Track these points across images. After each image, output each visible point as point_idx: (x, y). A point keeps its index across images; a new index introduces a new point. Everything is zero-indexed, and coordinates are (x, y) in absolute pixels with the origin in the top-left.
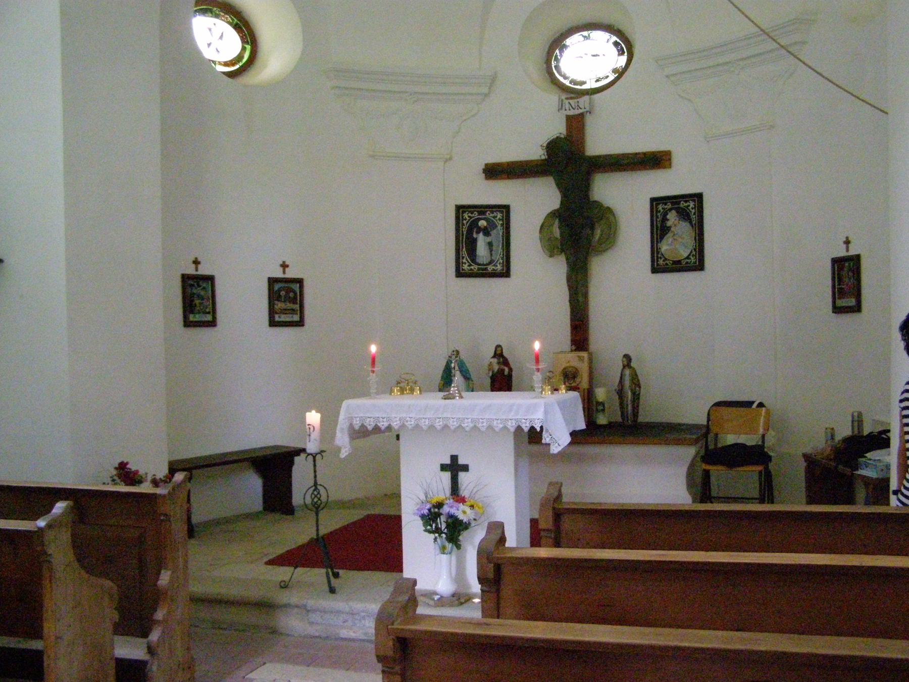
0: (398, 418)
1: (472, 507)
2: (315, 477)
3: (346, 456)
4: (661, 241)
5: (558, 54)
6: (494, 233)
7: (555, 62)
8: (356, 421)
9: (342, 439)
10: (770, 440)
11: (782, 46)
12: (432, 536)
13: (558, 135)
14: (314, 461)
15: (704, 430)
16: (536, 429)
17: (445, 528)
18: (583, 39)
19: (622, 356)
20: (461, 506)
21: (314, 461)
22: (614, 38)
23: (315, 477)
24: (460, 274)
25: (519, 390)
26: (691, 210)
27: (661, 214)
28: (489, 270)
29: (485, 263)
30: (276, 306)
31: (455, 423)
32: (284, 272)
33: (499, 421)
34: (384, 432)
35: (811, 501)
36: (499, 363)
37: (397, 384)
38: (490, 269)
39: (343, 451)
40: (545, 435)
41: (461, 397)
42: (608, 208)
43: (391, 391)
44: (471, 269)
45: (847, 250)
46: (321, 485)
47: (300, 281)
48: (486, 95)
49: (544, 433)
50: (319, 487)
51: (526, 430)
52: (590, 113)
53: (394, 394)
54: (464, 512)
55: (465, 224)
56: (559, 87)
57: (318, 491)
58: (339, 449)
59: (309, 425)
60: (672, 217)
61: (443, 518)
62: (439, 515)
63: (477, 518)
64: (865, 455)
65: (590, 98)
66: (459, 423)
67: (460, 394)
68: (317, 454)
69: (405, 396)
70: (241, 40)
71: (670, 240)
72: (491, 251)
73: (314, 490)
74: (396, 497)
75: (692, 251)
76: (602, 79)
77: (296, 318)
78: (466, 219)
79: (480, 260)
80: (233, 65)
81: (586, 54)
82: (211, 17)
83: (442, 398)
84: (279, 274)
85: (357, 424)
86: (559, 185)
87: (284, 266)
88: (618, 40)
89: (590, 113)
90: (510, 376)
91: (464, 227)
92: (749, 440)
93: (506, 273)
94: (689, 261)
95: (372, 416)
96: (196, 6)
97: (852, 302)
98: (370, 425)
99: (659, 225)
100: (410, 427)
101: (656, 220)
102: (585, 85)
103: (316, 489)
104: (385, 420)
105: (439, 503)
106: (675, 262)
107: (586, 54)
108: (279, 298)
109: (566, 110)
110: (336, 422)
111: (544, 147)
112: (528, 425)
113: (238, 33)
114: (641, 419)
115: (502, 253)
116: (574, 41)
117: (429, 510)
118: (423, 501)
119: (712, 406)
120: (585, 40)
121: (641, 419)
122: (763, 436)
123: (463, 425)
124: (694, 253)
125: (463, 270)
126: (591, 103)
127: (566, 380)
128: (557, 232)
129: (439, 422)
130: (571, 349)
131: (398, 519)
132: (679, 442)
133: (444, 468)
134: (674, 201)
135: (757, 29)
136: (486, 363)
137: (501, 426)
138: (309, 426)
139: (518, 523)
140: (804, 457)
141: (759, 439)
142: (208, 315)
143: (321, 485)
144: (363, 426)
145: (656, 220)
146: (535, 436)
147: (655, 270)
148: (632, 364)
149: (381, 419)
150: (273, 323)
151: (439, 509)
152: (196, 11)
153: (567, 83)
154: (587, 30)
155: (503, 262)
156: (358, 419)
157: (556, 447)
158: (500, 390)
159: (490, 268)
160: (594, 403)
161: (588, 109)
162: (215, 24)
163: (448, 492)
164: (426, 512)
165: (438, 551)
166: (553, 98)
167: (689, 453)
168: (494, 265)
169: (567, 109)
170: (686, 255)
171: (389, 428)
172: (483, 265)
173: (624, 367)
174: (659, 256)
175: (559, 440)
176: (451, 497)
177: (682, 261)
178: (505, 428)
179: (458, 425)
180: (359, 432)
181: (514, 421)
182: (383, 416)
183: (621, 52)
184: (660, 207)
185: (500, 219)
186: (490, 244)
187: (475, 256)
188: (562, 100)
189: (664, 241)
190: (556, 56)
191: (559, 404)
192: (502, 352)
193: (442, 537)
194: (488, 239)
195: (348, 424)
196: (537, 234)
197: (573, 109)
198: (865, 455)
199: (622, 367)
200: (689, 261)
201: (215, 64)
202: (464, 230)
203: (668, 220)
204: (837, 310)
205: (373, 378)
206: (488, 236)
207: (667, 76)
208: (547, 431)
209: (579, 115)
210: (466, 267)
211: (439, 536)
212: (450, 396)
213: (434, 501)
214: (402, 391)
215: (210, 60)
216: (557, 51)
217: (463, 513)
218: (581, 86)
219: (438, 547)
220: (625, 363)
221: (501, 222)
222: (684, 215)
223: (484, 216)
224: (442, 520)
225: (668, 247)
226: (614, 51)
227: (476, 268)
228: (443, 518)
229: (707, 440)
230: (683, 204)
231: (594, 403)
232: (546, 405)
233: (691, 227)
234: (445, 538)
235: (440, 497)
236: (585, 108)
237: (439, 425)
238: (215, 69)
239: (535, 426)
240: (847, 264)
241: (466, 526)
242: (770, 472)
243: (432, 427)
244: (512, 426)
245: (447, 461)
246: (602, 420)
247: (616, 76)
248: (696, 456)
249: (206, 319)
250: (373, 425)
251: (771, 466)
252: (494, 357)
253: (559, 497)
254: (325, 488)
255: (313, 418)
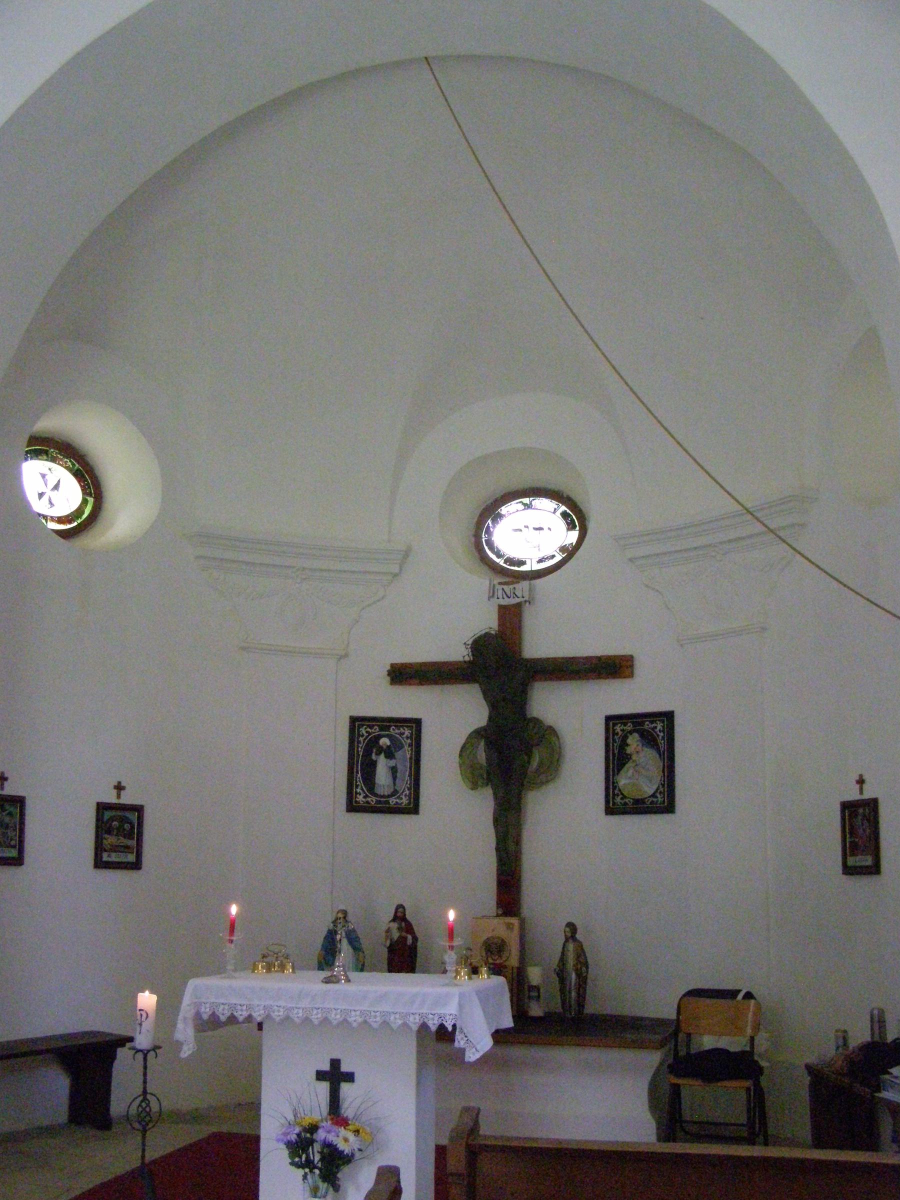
0: (262, 1006)
1: (357, 1132)
2: (145, 1082)
3: (189, 1056)
4: (617, 774)
5: (491, 525)
6: (399, 754)
7: (486, 536)
8: (206, 1008)
9: (185, 1032)
10: (762, 1043)
11: (772, 531)
12: (300, 1172)
13: (487, 631)
14: (145, 1059)
15: (671, 1030)
16: (447, 1028)
17: (319, 1161)
18: (523, 507)
19: (564, 924)
20: (342, 1131)
21: (145, 1059)
22: (563, 508)
23: (145, 1082)
24: (353, 807)
25: (424, 972)
26: (658, 733)
27: (619, 738)
28: (391, 803)
29: (386, 794)
30: (105, 841)
31: (338, 1016)
32: (119, 797)
33: (397, 1016)
34: (240, 1023)
35: (818, 1143)
36: (400, 929)
37: (263, 958)
38: (392, 802)
39: (185, 1048)
40: (458, 1036)
41: (348, 980)
42: (550, 727)
43: (254, 968)
44: (368, 802)
45: (861, 792)
46: (152, 1094)
47: (139, 810)
48: (395, 575)
49: (457, 1033)
50: (149, 1097)
51: (434, 1028)
52: (530, 603)
53: (258, 972)
54: (346, 1140)
55: (362, 742)
56: (490, 567)
57: (147, 1102)
58: (179, 1045)
59: (140, 1010)
60: (634, 741)
61: (317, 1147)
62: (311, 1142)
63: (364, 1149)
64: (889, 1070)
65: (530, 584)
66: (343, 1016)
67: (346, 973)
68: (148, 1051)
69: (273, 975)
70: (82, 490)
71: (631, 771)
72: (394, 778)
73: (142, 1101)
74: (254, 1107)
75: (659, 787)
76: (546, 559)
77: (131, 858)
78: (363, 736)
79: (379, 791)
80: (70, 523)
81: (527, 527)
82: (46, 460)
83: (322, 981)
84: (111, 798)
85: (206, 1013)
86: (485, 694)
87: (119, 788)
88: (568, 511)
89: (530, 603)
90: (413, 949)
91: (360, 745)
92: (734, 1044)
93: (413, 808)
94: (655, 800)
95: (226, 1001)
96: (28, 446)
97: (868, 861)
98: (223, 1014)
99: (616, 752)
100: (278, 1019)
101: (613, 745)
102: (525, 566)
103: (145, 1099)
104: (244, 1008)
105: (312, 1125)
106: (637, 801)
107: (527, 527)
108: (109, 832)
109: (498, 598)
110: (177, 1008)
111: (468, 645)
112: (436, 1022)
113: (79, 482)
114: (591, 1008)
115: (409, 782)
116: (511, 509)
117: (299, 1135)
118: (291, 1123)
119: (684, 995)
120: (525, 509)
121: (591, 1008)
122: (752, 1039)
123: (348, 1019)
124: (662, 789)
125: (356, 802)
126: (531, 590)
127: (489, 954)
128: (482, 756)
129: (317, 1014)
130: (497, 914)
131: (256, 1140)
132: (640, 1045)
133: (321, 1076)
134: (637, 721)
135: (741, 508)
136: (384, 927)
137: (400, 1022)
138: (142, 1012)
139: (419, 1170)
140: (810, 1073)
141: (747, 1043)
142: (13, 850)
143: (152, 1094)
144: (213, 1014)
145: (613, 745)
146: (445, 1035)
147: (611, 810)
148: (578, 936)
149: (239, 1006)
150: (99, 864)
151: (312, 1134)
152: (27, 452)
153: (501, 562)
154: (529, 497)
155: (410, 793)
156: (208, 1005)
157: (474, 1054)
158: (400, 971)
159: (393, 801)
160: (526, 987)
161: (526, 598)
162: (50, 469)
163: (325, 1109)
164: (293, 1137)
165: (308, 1193)
166: (482, 582)
167: (653, 1059)
168: (399, 798)
169: (500, 596)
170: (651, 792)
171: (249, 1018)
172: (383, 796)
173: (567, 940)
174: (616, 792)
175: (478, 1044)
176: (329, 1117)
177: (646, 800)
178: (405, 1024)
179: (341, 1019)
180: (207, 1022)
181: (417, 1017)
182: (243, 1002)
183: (571, 526)
184: (618, 728)
185: (407, 738)
186: (394, 770)
187: (374, 784)
188: (494, 586)
189: (622, 772)
190: (488, 527)
191: (478, 993)
192: (405, 915)
193: (314, 1173)
194: (392, 763)
195: (193, 1011)
196: (456, 759)
197: (508, 596)
198: (889, 1070)
199: (564, 940)
200: (655, 800)
201: (46, 521)
202: (360, 749)
203: (627, 745)
204: (848, 870)
205: (231, 951)
206: (391, 759)
207: (630, 560)
208: (462, 1031)
209: (514, 605)
210: (360, 798)
211: (311, 1171)
212: (334, 979)
213: (306, 1122)
214: (269, 968)
215: (40, 515)
216: (490, 521)
217: (345, 1140)
218: (519, 567)
219: (308, 1188)
220: (569, 935)
221: (409, 741)
222: (649, 740)
223: (387, 733)
224: (315, 1150)
225: (627, 781)
226: (562, 524)
227: (374, 800)
228: (317, 1147)
229: (676, 1041)
230: (647, 726)
231: (526, 987)
232: (462, 996)
233: (658, 756)
234: (319, 1175)
235: (316, 1117)
236: (523, 597)
237: (316, 1017)
238: (46, 526)
239: (445, 1023)
240: (861, 811)
241: (347, 1159)
242: (762, 1089)
243: (307, 1020)
244: (414, 1022)
245: (326, 1067)
246: (536, 1010)
247: (564, 556)
248: (661, 1064)
249: (11, 855)
250: (228, 1014)
251: (764, 1082)
252: (394, 920)
253: (474, 1129)
254: (158, 1100)
255: (147, 1000)
